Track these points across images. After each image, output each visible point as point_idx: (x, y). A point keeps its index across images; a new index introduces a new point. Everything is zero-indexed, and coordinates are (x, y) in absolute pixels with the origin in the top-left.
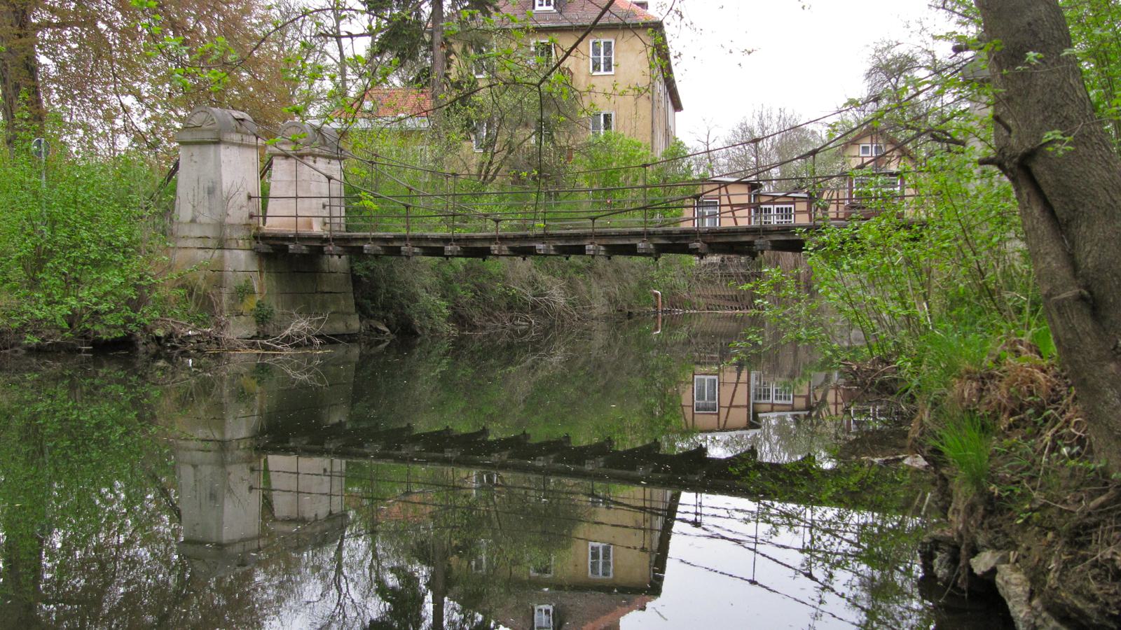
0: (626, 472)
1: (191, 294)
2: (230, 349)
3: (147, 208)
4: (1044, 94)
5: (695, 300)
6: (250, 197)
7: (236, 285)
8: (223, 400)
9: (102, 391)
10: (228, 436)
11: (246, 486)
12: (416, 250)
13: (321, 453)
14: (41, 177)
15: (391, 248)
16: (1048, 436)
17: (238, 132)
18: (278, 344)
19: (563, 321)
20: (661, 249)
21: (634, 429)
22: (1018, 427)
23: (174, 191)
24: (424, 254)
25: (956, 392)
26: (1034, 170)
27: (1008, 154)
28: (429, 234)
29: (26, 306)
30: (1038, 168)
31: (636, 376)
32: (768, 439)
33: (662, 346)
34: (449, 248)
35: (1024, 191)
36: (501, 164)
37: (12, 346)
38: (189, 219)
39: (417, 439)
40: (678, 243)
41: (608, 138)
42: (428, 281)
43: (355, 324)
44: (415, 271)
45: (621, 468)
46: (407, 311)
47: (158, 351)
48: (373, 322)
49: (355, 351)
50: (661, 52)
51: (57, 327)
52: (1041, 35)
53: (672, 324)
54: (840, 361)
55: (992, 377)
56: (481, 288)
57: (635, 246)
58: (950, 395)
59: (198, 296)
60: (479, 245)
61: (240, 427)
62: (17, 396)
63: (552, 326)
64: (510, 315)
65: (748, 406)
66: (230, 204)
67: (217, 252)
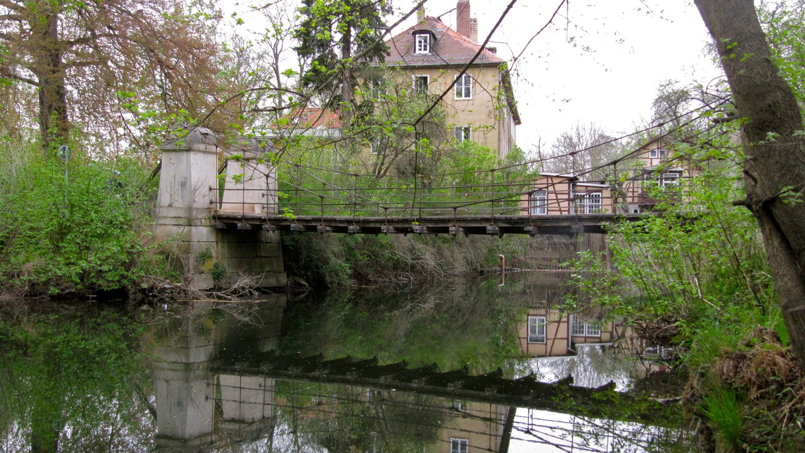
0: (477, 392)
1: (167, 258)
2: (194, 298)
3: (138, 197)
4: (780, 156)
5: (529, 261)
6: (211, 189)
7: (200, 251)
8: (188, 335)
9: (102, 327)
10: (191, 360)
11: (203, 398)
12: (328, 228)
13: (256, 373)
14: (64, 175)
15: (310, 226)
16: (786, 408)
17: (203, 143)
18: (228, 295)
19: (433, 277)
20: (503, 231)
21: (484, 355)
22: (764, 398)
23: (157, 184)
24: (333, 232)
25: (718, 367)
26: (774, 212)
27: (755, 199)
28: (338, 217)
29: (50, 267)
30: (776, 211)
31: (486, 317)
32: (581, 362)
33: (505, 295)
34: (351, 227)
35: (767, 227)
36: (390, 165)
37: (40, 294)
38: (167, 204)
39: (325, 365)
40: (515, 227)
41: (466, 146)
42: (336, 249)
43: (284, 280)
44: (327, 242)
45: (472, 389)
46: (321, 271)
47: (143, 298)
48: (297, 278)
49: (283, 299)
50: (505, 82)
51: (72, 281)
52: (778, 114)
53: (512, 278)
54: (633, 320)
55: (744, 357)
56: (375, 253)
57: (485, 228)
58: (713, 370)
59: (172, 259)
60: (373, 225)
61: (200, 354)
62: (43, 330)
63: (425, 280)
64: (395, 273)
65: (568, 339)
66: (197, 194)
67: (187, 228)
